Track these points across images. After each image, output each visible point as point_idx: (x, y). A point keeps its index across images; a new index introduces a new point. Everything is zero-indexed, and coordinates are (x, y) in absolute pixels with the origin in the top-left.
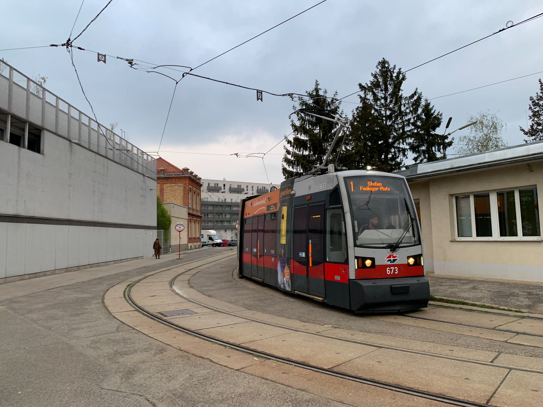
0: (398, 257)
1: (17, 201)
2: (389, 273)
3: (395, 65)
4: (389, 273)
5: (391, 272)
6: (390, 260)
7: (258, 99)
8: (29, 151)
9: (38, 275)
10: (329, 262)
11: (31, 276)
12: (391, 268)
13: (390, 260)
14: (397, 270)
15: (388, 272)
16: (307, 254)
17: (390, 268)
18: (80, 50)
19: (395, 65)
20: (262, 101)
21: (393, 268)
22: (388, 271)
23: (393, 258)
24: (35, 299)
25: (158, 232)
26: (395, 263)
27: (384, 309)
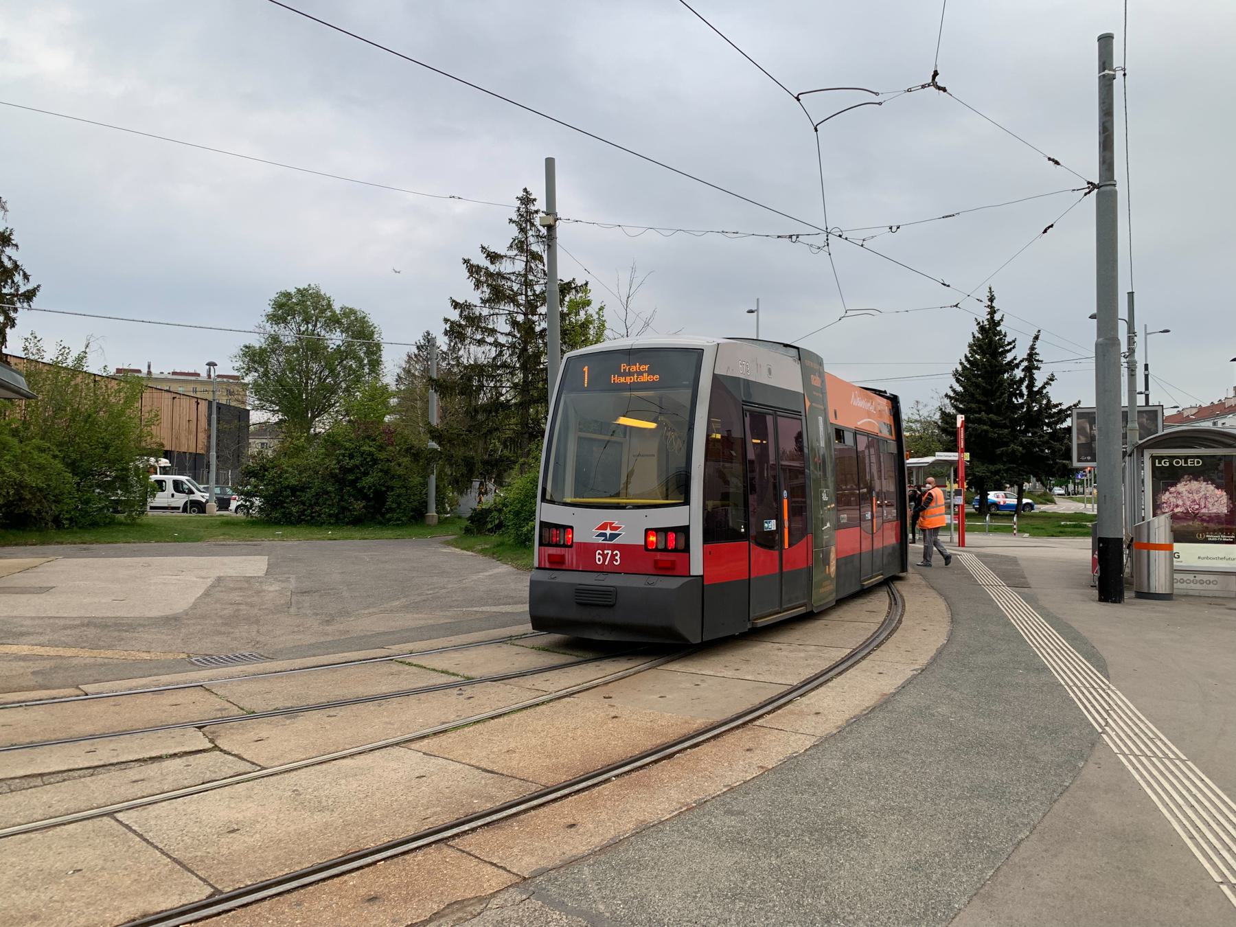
0: (594, 533)
5: (604, 561)
6: (604, 535)
12: (606, 552)
14: (618, 558)
15: (599, 560)
16: (780, 525)
17: (603, 552)
18: (1056, 159)
19: (483, 248)
21: (610, 552)
22: (597, 557)
26: (616, 541)
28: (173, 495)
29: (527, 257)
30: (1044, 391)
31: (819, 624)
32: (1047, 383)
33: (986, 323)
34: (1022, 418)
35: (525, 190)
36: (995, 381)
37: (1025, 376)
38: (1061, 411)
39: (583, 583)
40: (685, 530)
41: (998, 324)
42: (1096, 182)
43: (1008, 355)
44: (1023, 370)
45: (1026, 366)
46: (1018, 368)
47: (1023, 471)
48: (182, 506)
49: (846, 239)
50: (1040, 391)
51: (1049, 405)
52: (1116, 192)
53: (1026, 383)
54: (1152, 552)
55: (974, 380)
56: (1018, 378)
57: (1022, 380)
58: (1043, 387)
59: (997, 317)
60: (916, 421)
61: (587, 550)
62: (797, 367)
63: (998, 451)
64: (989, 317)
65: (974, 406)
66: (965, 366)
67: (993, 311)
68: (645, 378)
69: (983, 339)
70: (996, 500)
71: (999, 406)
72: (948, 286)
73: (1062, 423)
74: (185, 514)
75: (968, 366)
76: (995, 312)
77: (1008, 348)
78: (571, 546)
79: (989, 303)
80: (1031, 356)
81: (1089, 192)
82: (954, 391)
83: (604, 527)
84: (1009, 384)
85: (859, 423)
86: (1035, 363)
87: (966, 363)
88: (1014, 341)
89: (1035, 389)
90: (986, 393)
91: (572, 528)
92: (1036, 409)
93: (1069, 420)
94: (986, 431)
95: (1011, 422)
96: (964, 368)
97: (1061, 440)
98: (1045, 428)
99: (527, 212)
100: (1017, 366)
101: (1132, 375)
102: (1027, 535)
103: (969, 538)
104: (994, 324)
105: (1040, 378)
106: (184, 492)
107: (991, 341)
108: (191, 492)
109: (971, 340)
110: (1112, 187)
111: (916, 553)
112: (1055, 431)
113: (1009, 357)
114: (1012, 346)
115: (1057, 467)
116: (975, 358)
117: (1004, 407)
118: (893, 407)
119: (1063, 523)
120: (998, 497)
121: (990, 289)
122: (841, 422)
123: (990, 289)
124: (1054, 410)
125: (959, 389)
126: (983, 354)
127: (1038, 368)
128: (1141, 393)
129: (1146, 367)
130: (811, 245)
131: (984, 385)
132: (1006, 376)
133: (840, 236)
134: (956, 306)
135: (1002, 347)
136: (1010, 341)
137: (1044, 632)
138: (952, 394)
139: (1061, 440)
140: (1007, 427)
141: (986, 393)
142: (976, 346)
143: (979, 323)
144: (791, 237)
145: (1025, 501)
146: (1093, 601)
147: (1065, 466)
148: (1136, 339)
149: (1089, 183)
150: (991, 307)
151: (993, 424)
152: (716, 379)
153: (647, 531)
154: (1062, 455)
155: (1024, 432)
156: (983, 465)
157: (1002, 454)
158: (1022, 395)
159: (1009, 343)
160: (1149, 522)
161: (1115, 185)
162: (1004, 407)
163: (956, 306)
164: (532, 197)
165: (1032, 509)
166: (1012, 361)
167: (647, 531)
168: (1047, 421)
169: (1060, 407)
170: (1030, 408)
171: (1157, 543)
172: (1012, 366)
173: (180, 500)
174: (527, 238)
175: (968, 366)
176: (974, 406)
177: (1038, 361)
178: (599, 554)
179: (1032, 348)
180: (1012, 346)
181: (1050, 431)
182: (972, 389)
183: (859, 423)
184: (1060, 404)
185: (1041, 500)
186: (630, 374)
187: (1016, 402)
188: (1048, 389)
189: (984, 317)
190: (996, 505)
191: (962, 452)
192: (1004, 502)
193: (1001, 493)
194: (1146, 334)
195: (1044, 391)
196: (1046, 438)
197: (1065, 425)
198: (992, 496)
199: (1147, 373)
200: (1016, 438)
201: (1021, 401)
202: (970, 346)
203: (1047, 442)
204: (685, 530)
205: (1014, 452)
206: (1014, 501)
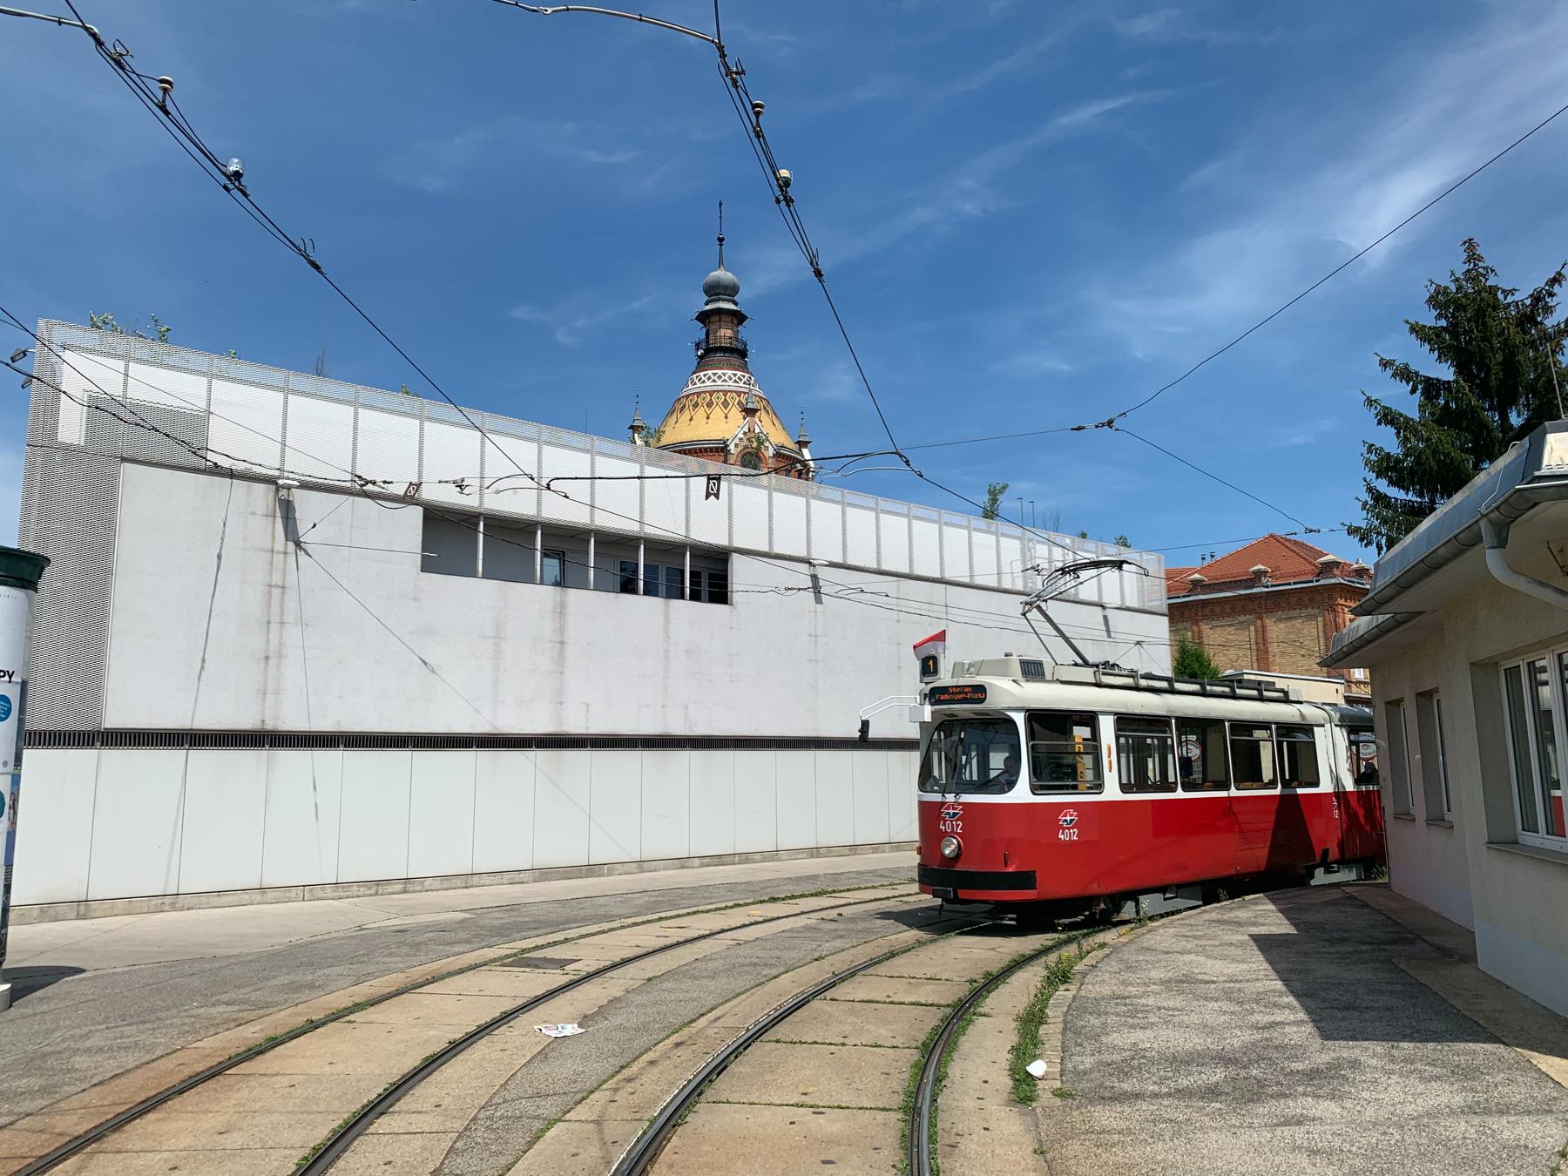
1: (663, 706)
7: (708, 496)
8: (691, 602)
9: (725, 859)
11: (705, 861)
20: (718, 498)
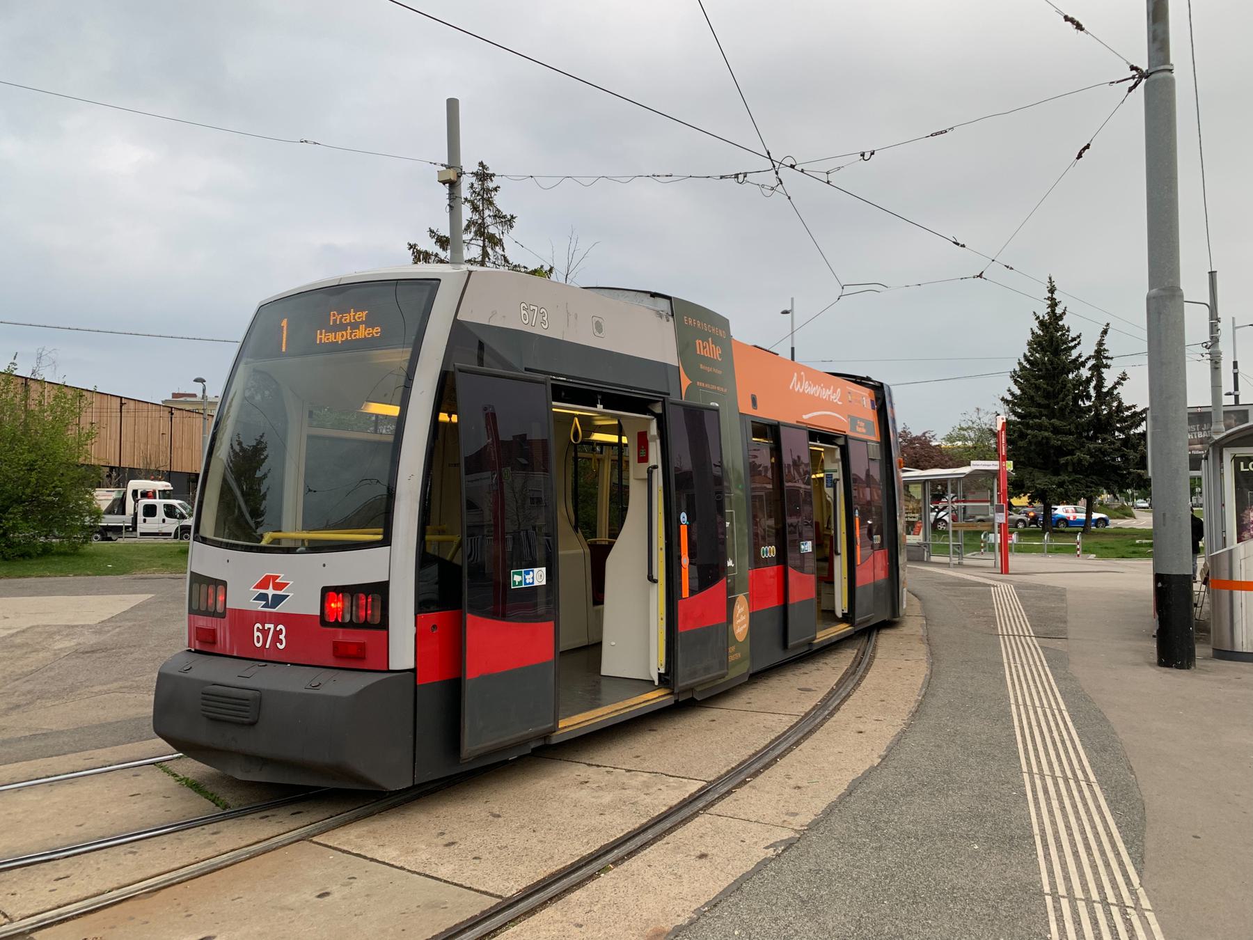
2: (258, 642)
3: (431, 231)
4: (258, 642)
10: (550, 620)
12: (267, 626)
13: (263, 597)
14: (282, 637)
17: (264, 627)
19: (431, 231)
21: (272, 626)
22: (256, 634)
23: (266, 595)
24: (57, 702)
25: (317, 616)
26: (279, 609)
27: (604, 521)
28: (164, 521)
29: (484, 241)
30: (1115, 392)
31: (701, 719)
32: (1118, 383)
33: (1047, 317)
34: (1089, 422)
35: (481, 164)
36: (1058, 382)
37: (1092, 376)
38: (1135, 414)
39: (219, 681)
40: (381, 589)
41: (1061, 317)
42: (1144, 67)
43: (1073, 352)
44: (1090, 369)
45: (1093, 365)
46: (1084, 366)
47: (1092, 483)
48: (173, 531)
49: (802, 171)
50: (1110, 392)
51: (1120, 408)
52: (1172, 80)
53: (1093, 384)
54: (1237, 593)
55: (1033, 381)
56: (1084, 378)
57: (1089, 380)
58: (1114, 387)
59: (1059, 311)
60: (969, 428)
61: (244, 620)
62: (669, 328)
63: (1062, 461)
64: (1049, 310)
65: (1033, 410)
66: (1024, 367)
67: (1054, 304)
68: (362, 333)
69: (1043, 336)
70: (1065, 515)
71: (1062, 410)
72: (963, 246)
73: (1136, 428)
74: (175, 541)
75: (1028, 366)
76: (1056, 305)
77: (1072, 344)
78: (222, 615)
79: (1050, 295)
80: (1099, 353)
81: (1136, 85)
82: (1012, 394)
83: (264, 584)
84: (1073, 385)
85: (805, 417)
86: (1104, 360)
87: (1024, 363)
88: (1079, 337)
89: (1105, 390)
90: (1047, 395)
91: (224, 583)
92: (1105, 412)
93: (1144, 423)
94: (1047, 438)
95: (1077, 428)
96: (1023, 368)
97: (1134, 448)
98: (1117, 434)
99: (483, 189)
100: (1083, 364)
101: (1217, 368)
102: (1093, 556)
103: (1015, 561)
104: (1055, 318)
105: (1110, 377)
106: (176, 517)
107: (1052, 338)
108: (182, 517)
109: (1030, 337)
110: (1168, 74)
111: (943, 584)
112: (1128, 438)
113: (1074, 354)
114: (1076, 342)
115: (1131, 478)
116: (1036, 358)
117: (1068, 410)
118: (877, 399)
119: (1137, 541)
120: (1067, 512)
121: (1050, 278)
122: (767, 412)
123: (1050, 278)
124: (1126, 413)
125: (1018, 392)
126: (1044, 350)
127: (1107, 366)
128: (1229, 394)
129: (1235, 365)
130: (763, 186)
131: (1045, 386)
132: (1071, 376)
133: (792, 166)
134: (980, 276)
135: (1066, 343)
136: (1074, 336)
137: (1056, 734)
138: (1010, 398)
139: (1134, 448)
140: (1071, 433)
141: (1047, 395)
142: (1037, 344)
143: (1038, 318)
144: (737, 176)
145: (1095, 516)
146: (1150, 664)
147: (1140, 476)
148: (1220, 325)
149: (1133, 68)
150: (1052, 299)
151: (1056, 431)
152: (460, 330)
153: (326, 591)
154: (1137, 464)
155: (1094, 438)
156: (1045, 476)
157: (1066, 464)
158: (1089, 398)
159: (1074, 339)
160: (1231, 552)
161: (1171, 71)
162: (1068, 410)
163: (980, 276)
164: (490, 172)
165: (1107, 524)
166: (1076, 360)
167: (326, 591)
168: (1118, 425)
169: (1133, 410)
170: (1098, 414)
171: (1243, 580)
172: (1077, 364)
173: (172, 525)
174: (483, 219)
175: (1028, 366)
176: (1033, 410)
177: (1107, 358)
178: (258, 630)
179: (1100, 344)
180: (1076, 342)
181: (1122, 436)
182: (1032, 393)
183: (805, 417)
184: (1134, 406)
185: (1118, 514)
186: (343, 327)
187: (1082, 405)
188: (1119, 389)
189: (1043, 311)
190: (1065, 521)
191: (1003, 460)
192: (1075, 517)
193: (1071, 508)
194: (1235, 328)
195: (1115, 392)
196: (1118, 444)
197: (1140, 430)
198: (1061, 511)
199: (1236, 371)
200: (1083, 445)
201: (1088, 403)
202: (1029, 344)
203: (1119, 450)
204: (381, 589)
205: (1080, 461)
206: (1082, 516)
